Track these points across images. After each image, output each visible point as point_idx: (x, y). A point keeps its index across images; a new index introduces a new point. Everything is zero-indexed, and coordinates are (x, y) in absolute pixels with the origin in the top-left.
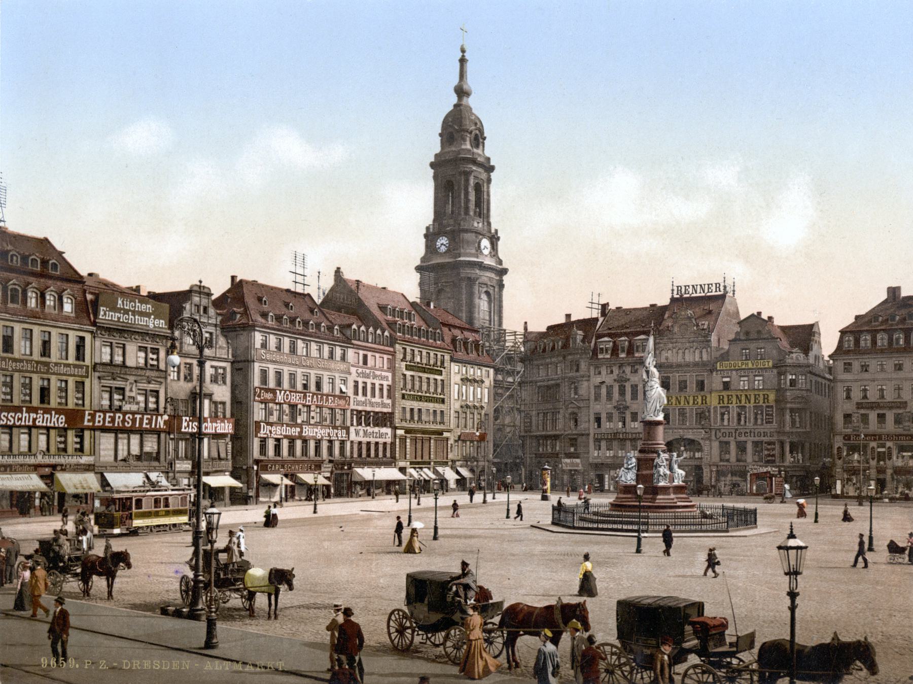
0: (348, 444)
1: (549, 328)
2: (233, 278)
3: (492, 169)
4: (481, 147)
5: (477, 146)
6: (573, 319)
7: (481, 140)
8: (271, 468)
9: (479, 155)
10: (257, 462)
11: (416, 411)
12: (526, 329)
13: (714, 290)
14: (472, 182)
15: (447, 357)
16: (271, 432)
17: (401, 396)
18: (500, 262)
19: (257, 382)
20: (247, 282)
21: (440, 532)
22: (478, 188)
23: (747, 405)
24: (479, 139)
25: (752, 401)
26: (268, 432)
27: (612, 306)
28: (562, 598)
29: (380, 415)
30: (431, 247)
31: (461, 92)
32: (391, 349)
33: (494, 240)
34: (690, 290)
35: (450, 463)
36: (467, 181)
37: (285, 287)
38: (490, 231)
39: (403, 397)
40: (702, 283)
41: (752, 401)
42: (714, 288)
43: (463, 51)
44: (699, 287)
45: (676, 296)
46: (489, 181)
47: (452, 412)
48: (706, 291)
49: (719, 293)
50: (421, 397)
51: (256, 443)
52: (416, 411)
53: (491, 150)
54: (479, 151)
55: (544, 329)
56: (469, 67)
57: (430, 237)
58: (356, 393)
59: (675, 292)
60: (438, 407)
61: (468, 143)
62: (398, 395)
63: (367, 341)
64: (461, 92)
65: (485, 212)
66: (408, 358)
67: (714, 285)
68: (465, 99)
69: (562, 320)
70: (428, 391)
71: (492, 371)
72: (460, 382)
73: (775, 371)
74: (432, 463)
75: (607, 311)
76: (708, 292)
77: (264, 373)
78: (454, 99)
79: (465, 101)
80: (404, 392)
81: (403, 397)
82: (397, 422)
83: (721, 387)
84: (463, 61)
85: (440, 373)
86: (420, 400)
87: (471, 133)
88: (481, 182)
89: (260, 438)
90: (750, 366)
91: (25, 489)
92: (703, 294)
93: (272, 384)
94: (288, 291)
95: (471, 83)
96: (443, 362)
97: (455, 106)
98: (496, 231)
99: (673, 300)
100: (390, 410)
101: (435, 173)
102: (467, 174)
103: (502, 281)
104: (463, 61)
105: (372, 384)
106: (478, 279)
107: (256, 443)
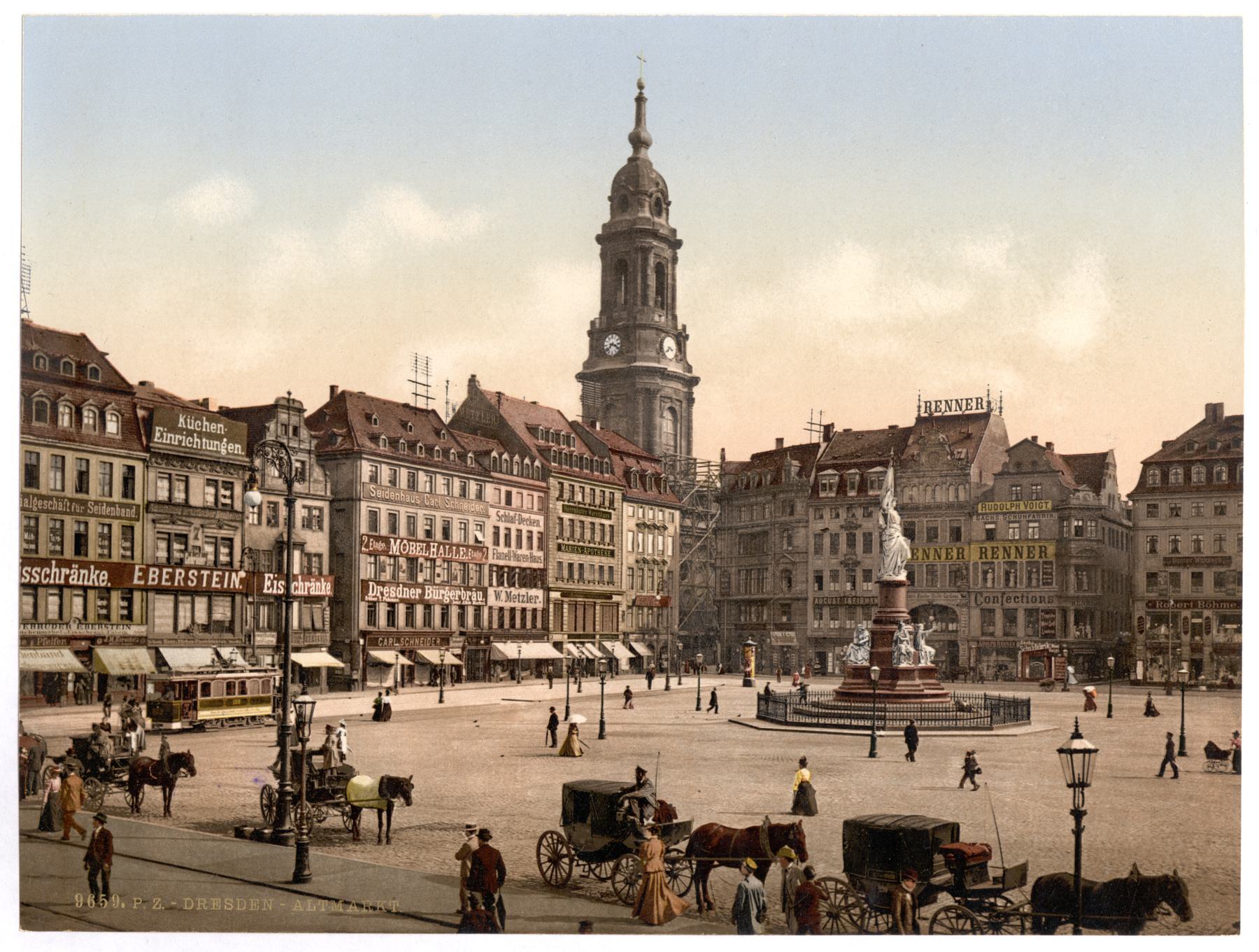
0: (486, 611)
1: (755, 457)
2: (333, 388)
3: (678, 244)
4: (664, 215)
5: (659, 214)
6: (786, 444)
7: (664, 206)
8: (382, 642)
9: (662, 226)
10: (364, 634)
11: (576, 567)
12: (723, 457)
13: (974, 407)
14: (652, 261)
15: (618, 495)
16: (382, 594)
17: (556, 547)
18: (689, 368)
19: (364, 528)
20: (351, 394)
21: (608, 729)
22: (660, 270)
23: (1018, 561)
24: (661, 205)
25: (1025, 555)
26: (379, 594)
27: (838, 428)
28: (770, 817)
29: (528, 572)
30: (596, 349)
31: (638, 142)
32: (544, 484)
33: (681, 339)
34: (943, 406)
35: (621, 637)
36: (645, 260)
37: (402, 401)
38: (675, 327)
39: (559, 548)
40: (958, 398)
41: (1025, 555)
42: (974, 404)
43: (641, 87)
44: (954, 402)
45: (923, 415)
46: (675, 260)
47: (624, 568)
48: (964, 408)
49: (980, 411)
50: (582, 548)
51: (363, 609)
52: (576, 567)
53: (678, 218)
54: (662, 221)
55: (747, 458)
56: (649, 108)
57: (596, 334)
58: (497, 543)
59: (923, 410)
60: (606, 561)
61: (647, 209)
62: (552, 545)
63: (512, 474)
64: (638, 142)
65: (669, 301)
66: (566, 496)
67: (974, 400)
68: (643, 150)
69: (772, 446)
70: (592, 540)
71: (677, 514)
72: (635, 528)
73: (1056, 515)
74: (598, 637)
75: (831, 434)
76: (967, 409)
77: (374, 515)
78: (628, 151)
79: (643, 153)
80: (560, 541)
81: (559, 548)
82: (551, 582)
83: (984, 536)
84: (640, 100)
85: (609, 516)
86: (582, 553)
87: (651, 196)
88: (664, 262)
89: (368, 601)
90: (1022, 508)
91: (55, 668)
92: (959, 413)
93: (384, 530)
94: (406, 406)
95: (652, 129)
96: (612, 502)
97: (630, 160)
98: (684, 327)
99: (920, 420)
100: (541, 566)
101: (602, 249)
102: (645, 251)
103: (691, 393)
104: (640, 100)
105: (518, 530)
106: (659, 391)
107: (363, 609)
